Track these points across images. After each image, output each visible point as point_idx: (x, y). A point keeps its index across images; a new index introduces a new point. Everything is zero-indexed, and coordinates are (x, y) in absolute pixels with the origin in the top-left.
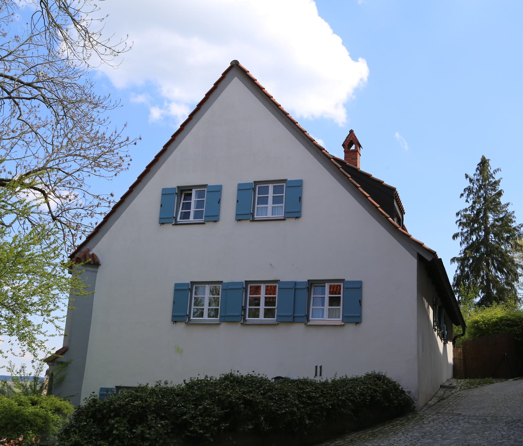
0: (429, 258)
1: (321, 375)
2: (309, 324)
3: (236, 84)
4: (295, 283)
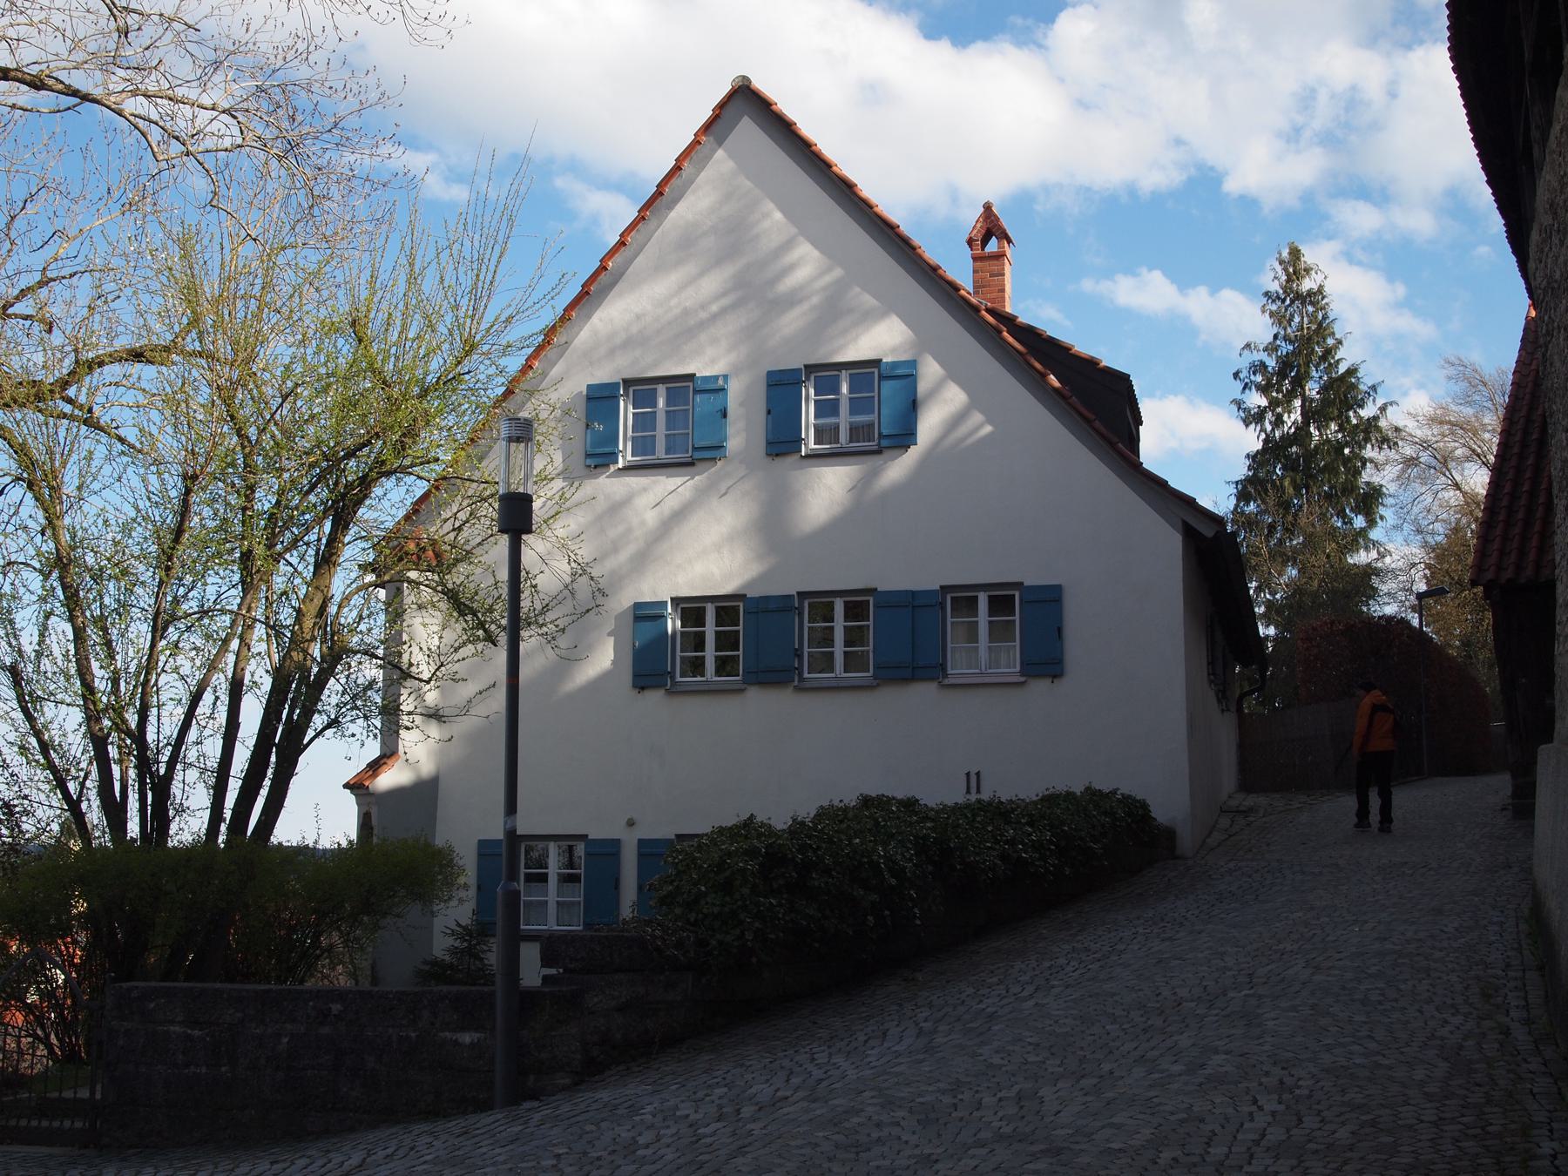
0: (1208, 531)
1: (978, 791)
2: (946, 682)
3: (747, 130)
4: (913, 593)
